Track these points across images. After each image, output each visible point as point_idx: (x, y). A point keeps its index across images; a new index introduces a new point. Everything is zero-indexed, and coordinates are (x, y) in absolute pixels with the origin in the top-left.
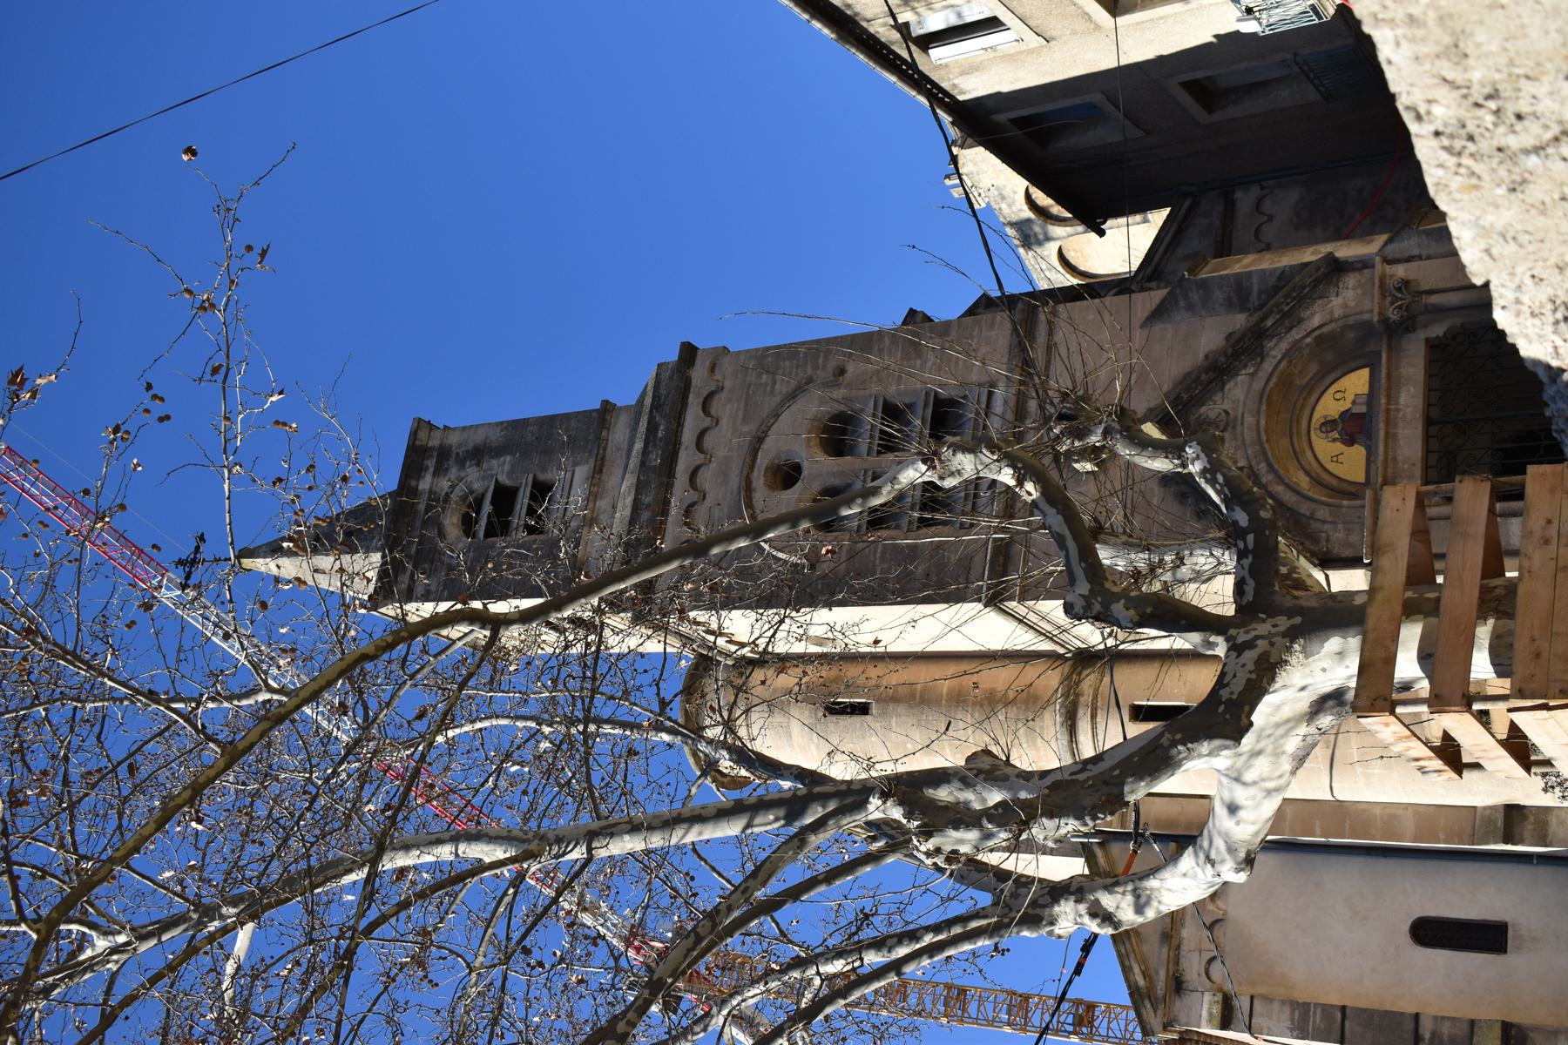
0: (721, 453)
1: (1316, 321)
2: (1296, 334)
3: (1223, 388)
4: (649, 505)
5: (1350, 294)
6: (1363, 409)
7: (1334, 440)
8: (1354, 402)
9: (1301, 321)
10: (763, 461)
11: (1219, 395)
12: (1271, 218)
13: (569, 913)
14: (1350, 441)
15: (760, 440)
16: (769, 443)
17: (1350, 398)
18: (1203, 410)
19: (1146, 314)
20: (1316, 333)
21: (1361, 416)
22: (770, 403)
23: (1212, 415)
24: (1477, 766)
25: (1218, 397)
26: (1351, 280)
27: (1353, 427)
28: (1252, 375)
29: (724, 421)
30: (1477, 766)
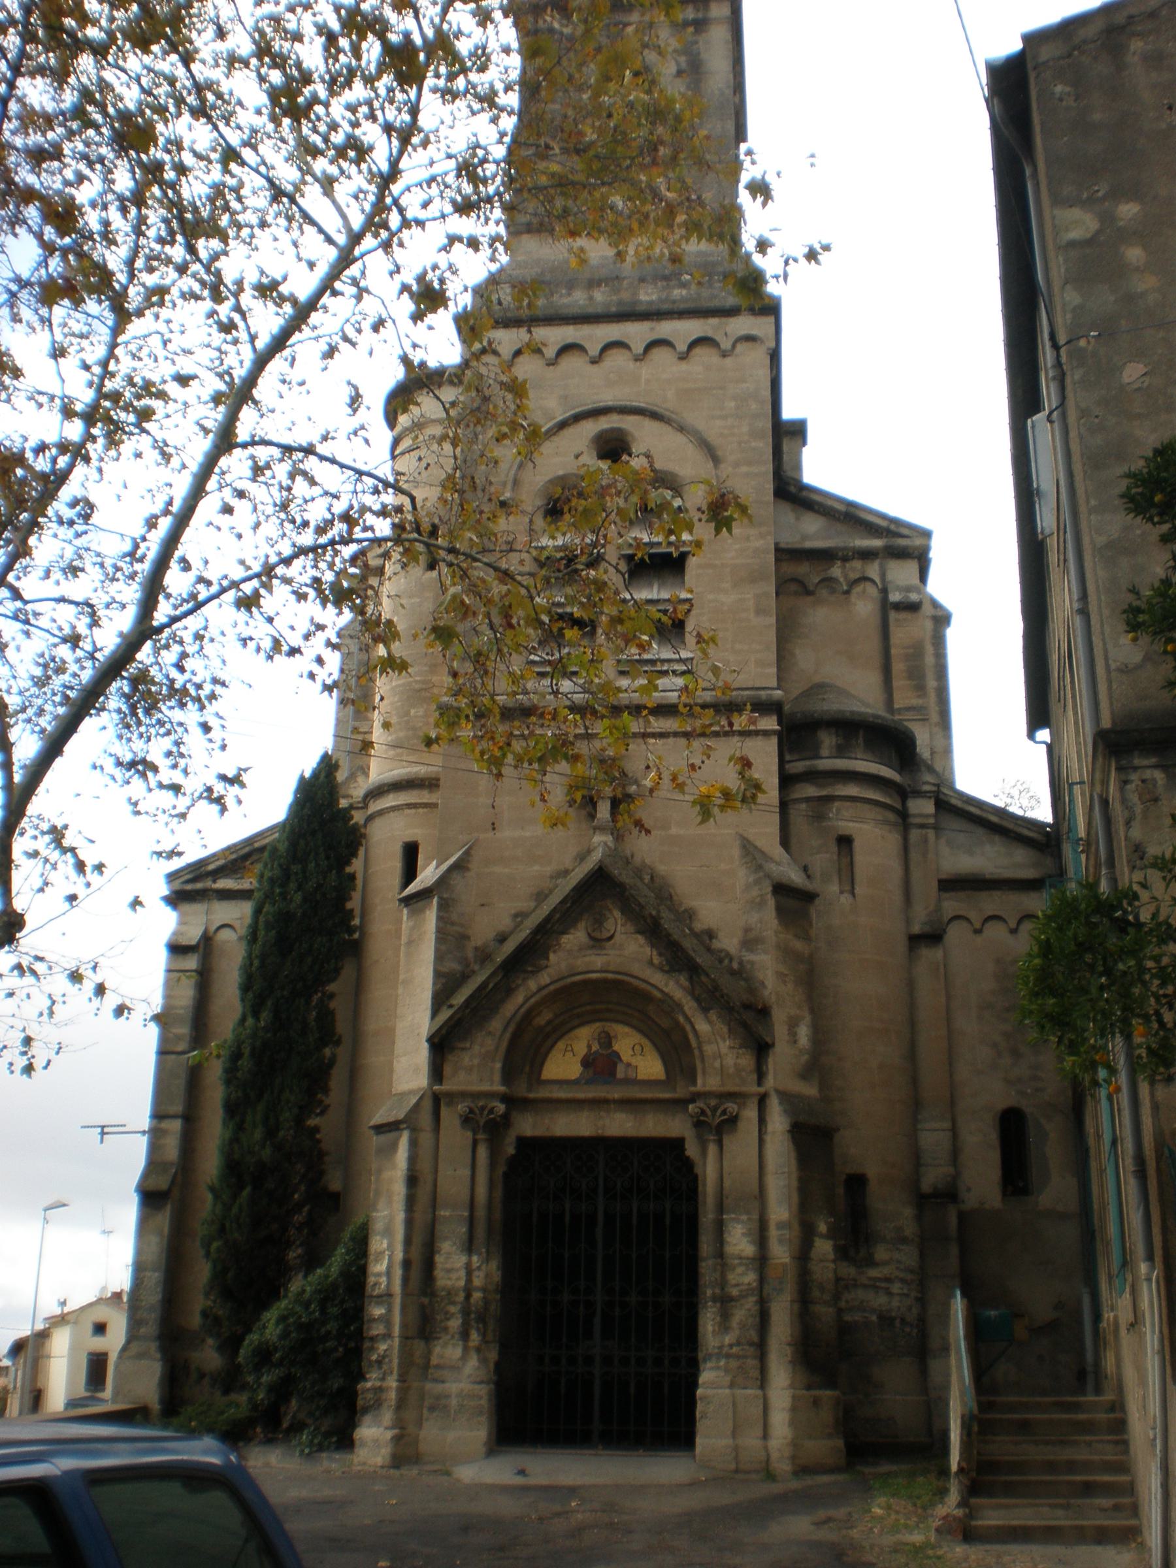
0: (645, 371)
1: (703, 1026)
2: (689, 1005)
3: (639, 932)
4: (591, 298)
5: (730, 1061)
6: (620, 1074)
7: (589, 1047)
8: (629, 1065)
9: (705, 1010)
10: (628, 423)
11: (632, 929)
12: (1013, 931)
13: (168, 95)
14: (586, 1063)
15: (655, 416)
16: (648, 424)
17: (634, 1061)
18: (617, 914)
19: (751, 838)
20: (688, 1028)
21: (613, 1073)
22: (696, 418)
23: (609, 925)
24: (349, 383)
25: (630, 928)
26: (747, 1061)
27: (601, 1065)
28: (651, 963)
29: (684, 366)
30: (349, 383)
